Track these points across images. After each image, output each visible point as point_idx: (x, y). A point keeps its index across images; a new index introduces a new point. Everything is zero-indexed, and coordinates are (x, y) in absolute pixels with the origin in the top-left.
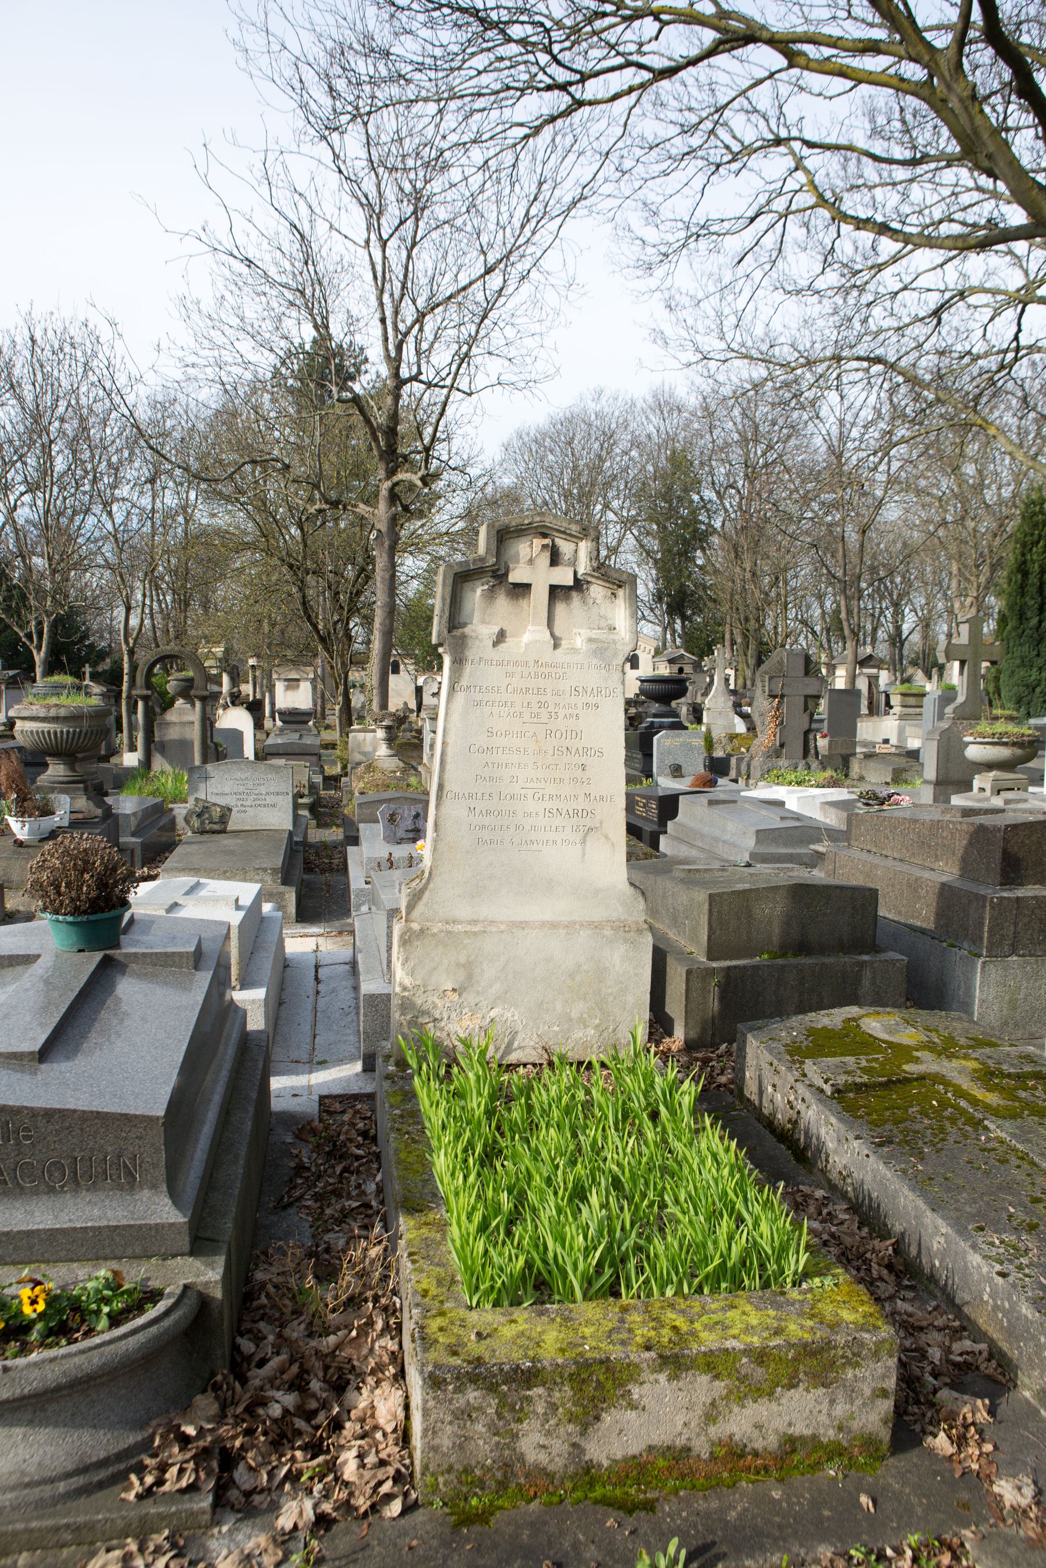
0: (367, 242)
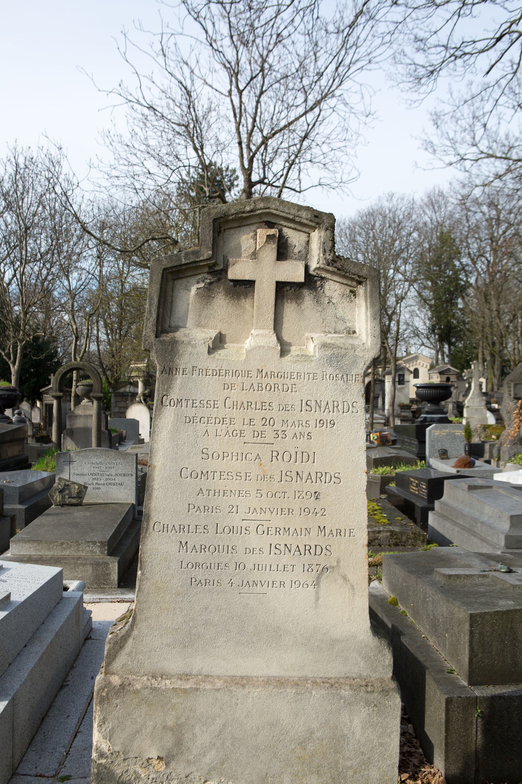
0: (230, 92)
